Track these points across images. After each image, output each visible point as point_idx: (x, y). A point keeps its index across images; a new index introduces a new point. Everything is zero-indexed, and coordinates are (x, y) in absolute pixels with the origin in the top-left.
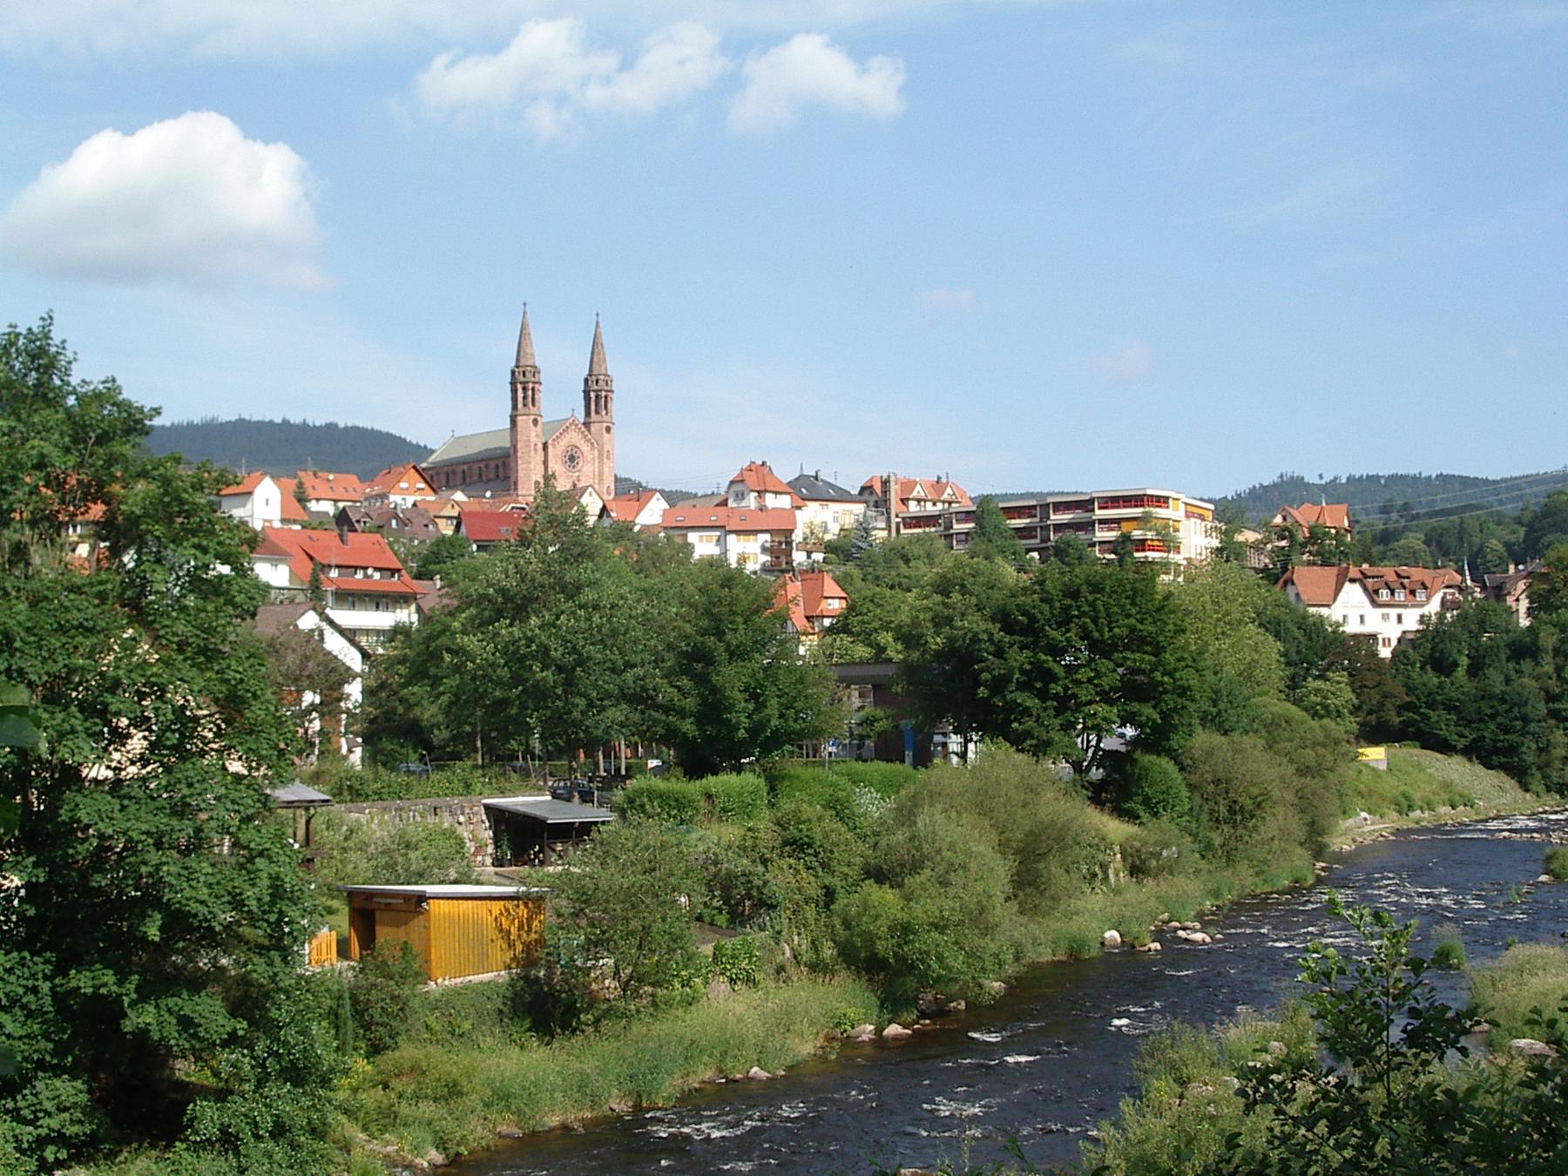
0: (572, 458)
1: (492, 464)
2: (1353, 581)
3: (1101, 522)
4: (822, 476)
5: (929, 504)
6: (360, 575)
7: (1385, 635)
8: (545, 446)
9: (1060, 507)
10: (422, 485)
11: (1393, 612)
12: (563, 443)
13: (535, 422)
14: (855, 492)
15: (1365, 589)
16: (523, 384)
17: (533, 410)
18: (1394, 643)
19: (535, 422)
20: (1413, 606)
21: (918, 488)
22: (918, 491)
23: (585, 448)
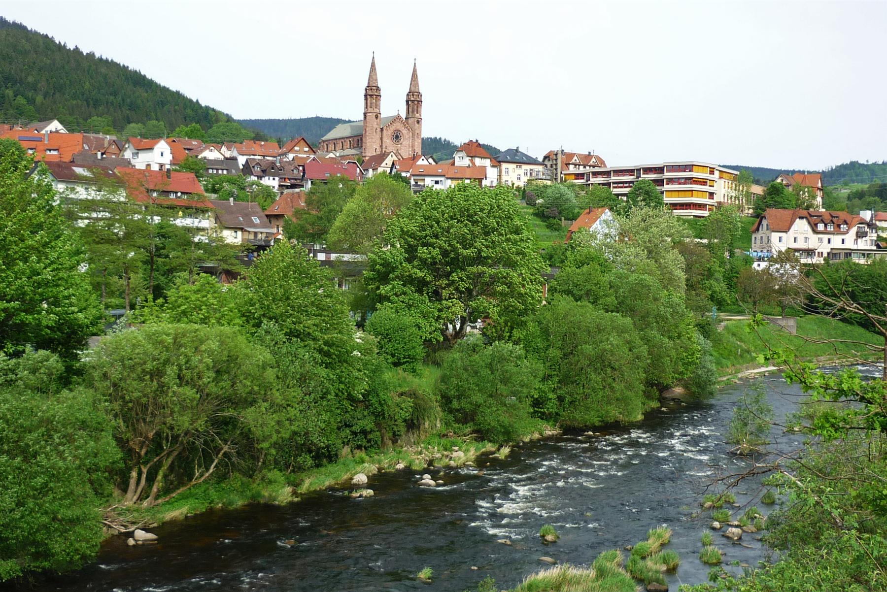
0: (397, 137)
1: (356, 139)
2: (801, 218)
3: (614, 183)
4: (520, 150)
5: (581, 167)
6: (172, 196)
7: (819, 250)
8: (382, 129)
9: (648, 170)
10: (307, 149)
11: (825, 237)
12: (392, 129)
13: (377, 117)
14: (540, 159)
15: (809, 223)
16: (372, 93)
17: (417, 115)
18: (825, 255)
19: (377, 117)
20: (838, 234)
21: (575, 158)
22: (575, 159)
23: (405, 132)
